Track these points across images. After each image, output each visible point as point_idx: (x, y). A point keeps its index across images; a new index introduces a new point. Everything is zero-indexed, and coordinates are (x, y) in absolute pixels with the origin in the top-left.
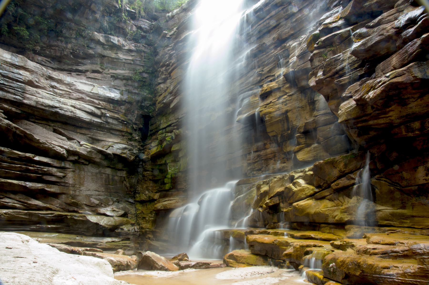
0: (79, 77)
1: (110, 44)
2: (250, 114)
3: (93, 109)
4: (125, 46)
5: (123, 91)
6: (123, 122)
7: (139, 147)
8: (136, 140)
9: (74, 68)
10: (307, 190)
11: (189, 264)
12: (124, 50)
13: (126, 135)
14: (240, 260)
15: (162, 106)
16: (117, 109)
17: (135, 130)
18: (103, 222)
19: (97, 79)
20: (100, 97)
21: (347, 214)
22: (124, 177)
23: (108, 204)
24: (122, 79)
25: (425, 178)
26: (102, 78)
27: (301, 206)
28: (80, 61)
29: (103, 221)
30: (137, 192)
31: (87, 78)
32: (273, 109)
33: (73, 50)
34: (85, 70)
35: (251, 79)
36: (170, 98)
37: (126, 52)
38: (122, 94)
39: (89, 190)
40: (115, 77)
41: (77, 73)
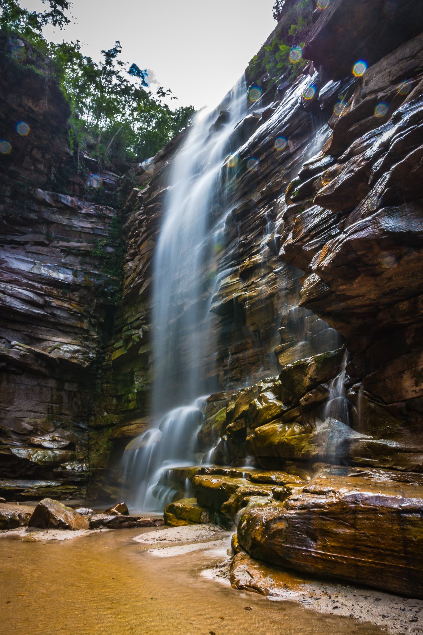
0: (14, 251)
1: (59, 205)
2: (226, 300)
3: (31, 295)
4: (81, 209)
5: (77, 271)
6: (76, 314)
7: (97, 349)
8: (94, 340)
9: (9, 238)
10: (274, 408)
11: (104, 520)
12: (81, 215)
13: (79, 332)
14: (180, 514)
15: (129, 292)
16: (68, 297)
17: (94, 326)
18: (36, 457)
19: (40, 254)
20: (43, 279)
21: (316, 445)
22: (75, 392)
23: (46, 431)
24: (76, 255)
25: (414, 388)
26: (49, 252)
27: (264, 431)
28: (17, 228)
29: (37, 456)
30: (92, 413)
31: (27, 252)
32: (253, 293)
33: (6, 213)
34: (24, 242)
35: (232, 252)
36: (138, 280)
37: (82, 217)
38: (75, 274)
39: (21, 410)
40: (67, 252)
41: (13, 246)
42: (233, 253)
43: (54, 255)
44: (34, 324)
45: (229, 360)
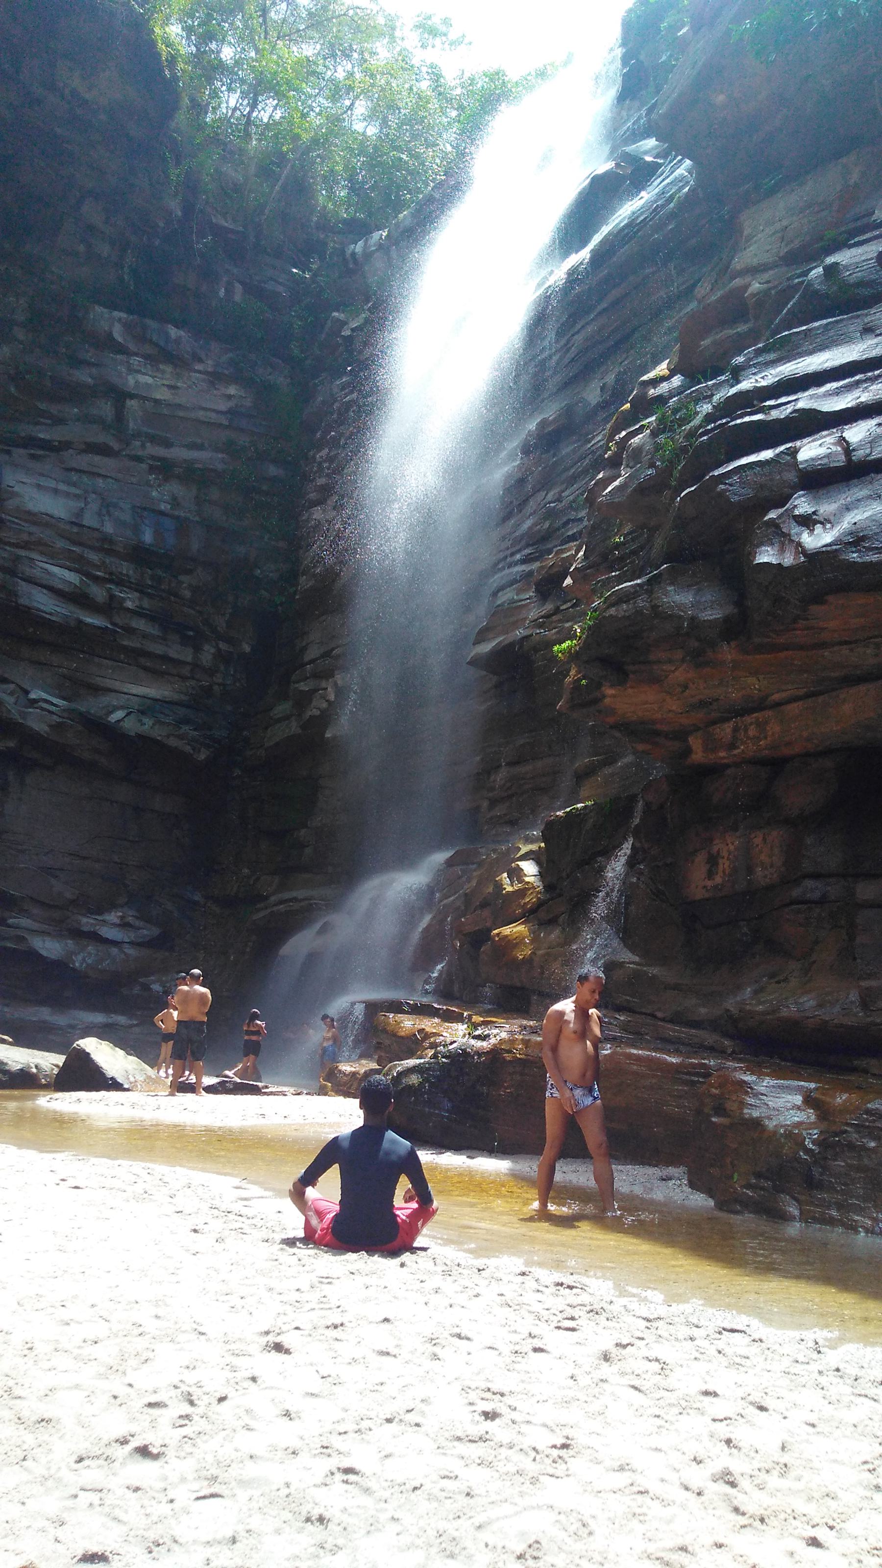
9: (25, 430)
18: (84, 959)
19: (99, 475)
28: (43, 406)
34: (60, 442)
35: (528, 523)
42: (530, 528)
43: (134, 480)
44: (83, 652)
45: (500, 777)
